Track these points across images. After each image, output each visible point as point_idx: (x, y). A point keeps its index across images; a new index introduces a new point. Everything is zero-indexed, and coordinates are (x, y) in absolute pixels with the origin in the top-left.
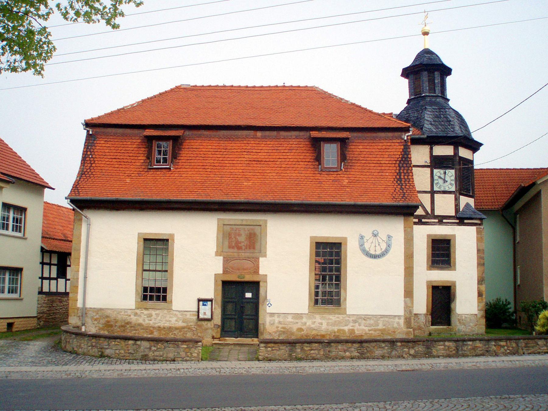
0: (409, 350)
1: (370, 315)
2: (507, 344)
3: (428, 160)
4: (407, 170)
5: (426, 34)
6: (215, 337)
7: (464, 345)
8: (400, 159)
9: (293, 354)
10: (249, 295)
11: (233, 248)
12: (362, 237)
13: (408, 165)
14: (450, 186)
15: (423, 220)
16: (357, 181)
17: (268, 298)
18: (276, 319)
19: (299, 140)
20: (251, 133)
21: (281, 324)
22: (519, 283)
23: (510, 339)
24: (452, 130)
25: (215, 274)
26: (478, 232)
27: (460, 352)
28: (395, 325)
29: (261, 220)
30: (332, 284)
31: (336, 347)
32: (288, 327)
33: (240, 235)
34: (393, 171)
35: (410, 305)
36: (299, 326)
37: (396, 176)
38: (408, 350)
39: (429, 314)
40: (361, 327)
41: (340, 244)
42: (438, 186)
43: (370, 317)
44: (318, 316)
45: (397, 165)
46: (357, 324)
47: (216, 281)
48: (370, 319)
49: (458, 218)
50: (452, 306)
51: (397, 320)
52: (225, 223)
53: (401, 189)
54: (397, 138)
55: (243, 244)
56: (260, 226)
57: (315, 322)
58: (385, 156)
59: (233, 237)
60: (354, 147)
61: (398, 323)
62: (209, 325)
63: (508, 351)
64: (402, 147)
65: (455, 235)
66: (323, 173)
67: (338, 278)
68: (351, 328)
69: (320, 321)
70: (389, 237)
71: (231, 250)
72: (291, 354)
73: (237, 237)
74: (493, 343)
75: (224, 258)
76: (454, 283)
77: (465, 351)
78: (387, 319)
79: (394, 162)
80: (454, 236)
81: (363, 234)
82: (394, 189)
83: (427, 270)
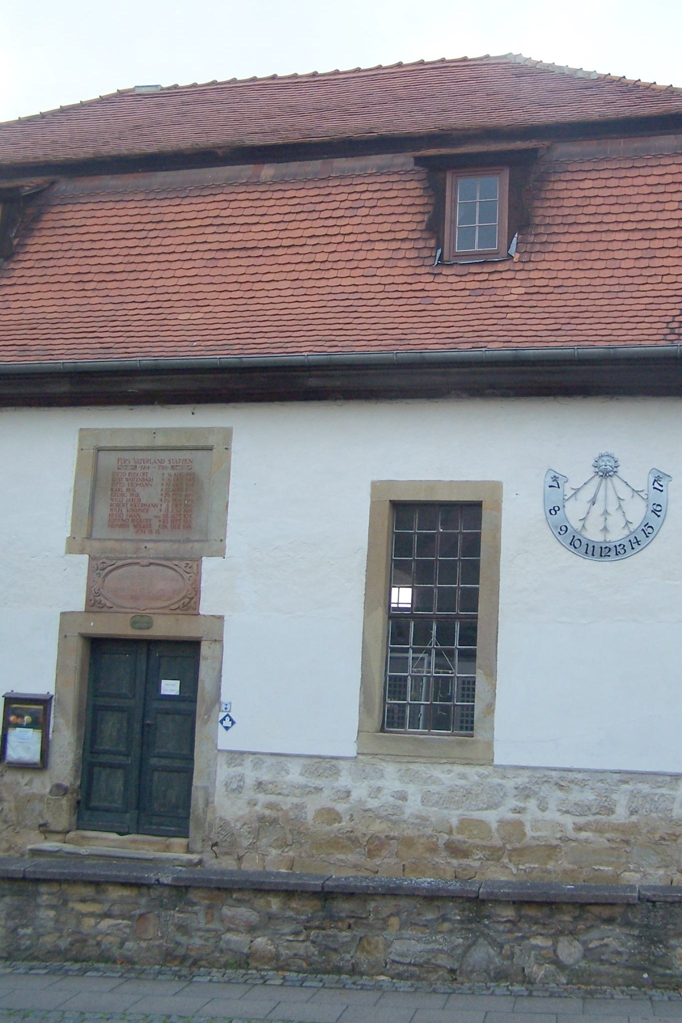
1: (579, 771)
6: (52, 827)
9: (22, 931)
10: (170, 687)
11: (121, 526)
12: (555, 479)
16: (557, 290)
17: (223, 699)
18: (250, 774)
19: (384, 179)
20: (246, 170)
21: (265, 792)
25: (63, 614)
29: (211, 430)
30: (450, 653)
31: (210, 907)
32: (287, 803)
33: (147, 482)
36: (323, 800)
41: (476, 507)
43: (580, 776)
44: (390, 769)
46: (532, 804)
47: (63, 636)
48: (582, 784)
52: (102, 444)
55: (154, 512)
56: (210, 449)
57: (379, 789)
58: (668, 206)
59: (124, 489)
60: (563, 185)
62: (41, 785)
66: (446, 271)
67: (470, 634)
68: (511, 816)
69: (398, 786)
70: (658, 481)
71: (118, 534)
72: (14, 930)
73: (138, 490)
75: (92, 559)
78: (645, 788)
81: (561, 470)
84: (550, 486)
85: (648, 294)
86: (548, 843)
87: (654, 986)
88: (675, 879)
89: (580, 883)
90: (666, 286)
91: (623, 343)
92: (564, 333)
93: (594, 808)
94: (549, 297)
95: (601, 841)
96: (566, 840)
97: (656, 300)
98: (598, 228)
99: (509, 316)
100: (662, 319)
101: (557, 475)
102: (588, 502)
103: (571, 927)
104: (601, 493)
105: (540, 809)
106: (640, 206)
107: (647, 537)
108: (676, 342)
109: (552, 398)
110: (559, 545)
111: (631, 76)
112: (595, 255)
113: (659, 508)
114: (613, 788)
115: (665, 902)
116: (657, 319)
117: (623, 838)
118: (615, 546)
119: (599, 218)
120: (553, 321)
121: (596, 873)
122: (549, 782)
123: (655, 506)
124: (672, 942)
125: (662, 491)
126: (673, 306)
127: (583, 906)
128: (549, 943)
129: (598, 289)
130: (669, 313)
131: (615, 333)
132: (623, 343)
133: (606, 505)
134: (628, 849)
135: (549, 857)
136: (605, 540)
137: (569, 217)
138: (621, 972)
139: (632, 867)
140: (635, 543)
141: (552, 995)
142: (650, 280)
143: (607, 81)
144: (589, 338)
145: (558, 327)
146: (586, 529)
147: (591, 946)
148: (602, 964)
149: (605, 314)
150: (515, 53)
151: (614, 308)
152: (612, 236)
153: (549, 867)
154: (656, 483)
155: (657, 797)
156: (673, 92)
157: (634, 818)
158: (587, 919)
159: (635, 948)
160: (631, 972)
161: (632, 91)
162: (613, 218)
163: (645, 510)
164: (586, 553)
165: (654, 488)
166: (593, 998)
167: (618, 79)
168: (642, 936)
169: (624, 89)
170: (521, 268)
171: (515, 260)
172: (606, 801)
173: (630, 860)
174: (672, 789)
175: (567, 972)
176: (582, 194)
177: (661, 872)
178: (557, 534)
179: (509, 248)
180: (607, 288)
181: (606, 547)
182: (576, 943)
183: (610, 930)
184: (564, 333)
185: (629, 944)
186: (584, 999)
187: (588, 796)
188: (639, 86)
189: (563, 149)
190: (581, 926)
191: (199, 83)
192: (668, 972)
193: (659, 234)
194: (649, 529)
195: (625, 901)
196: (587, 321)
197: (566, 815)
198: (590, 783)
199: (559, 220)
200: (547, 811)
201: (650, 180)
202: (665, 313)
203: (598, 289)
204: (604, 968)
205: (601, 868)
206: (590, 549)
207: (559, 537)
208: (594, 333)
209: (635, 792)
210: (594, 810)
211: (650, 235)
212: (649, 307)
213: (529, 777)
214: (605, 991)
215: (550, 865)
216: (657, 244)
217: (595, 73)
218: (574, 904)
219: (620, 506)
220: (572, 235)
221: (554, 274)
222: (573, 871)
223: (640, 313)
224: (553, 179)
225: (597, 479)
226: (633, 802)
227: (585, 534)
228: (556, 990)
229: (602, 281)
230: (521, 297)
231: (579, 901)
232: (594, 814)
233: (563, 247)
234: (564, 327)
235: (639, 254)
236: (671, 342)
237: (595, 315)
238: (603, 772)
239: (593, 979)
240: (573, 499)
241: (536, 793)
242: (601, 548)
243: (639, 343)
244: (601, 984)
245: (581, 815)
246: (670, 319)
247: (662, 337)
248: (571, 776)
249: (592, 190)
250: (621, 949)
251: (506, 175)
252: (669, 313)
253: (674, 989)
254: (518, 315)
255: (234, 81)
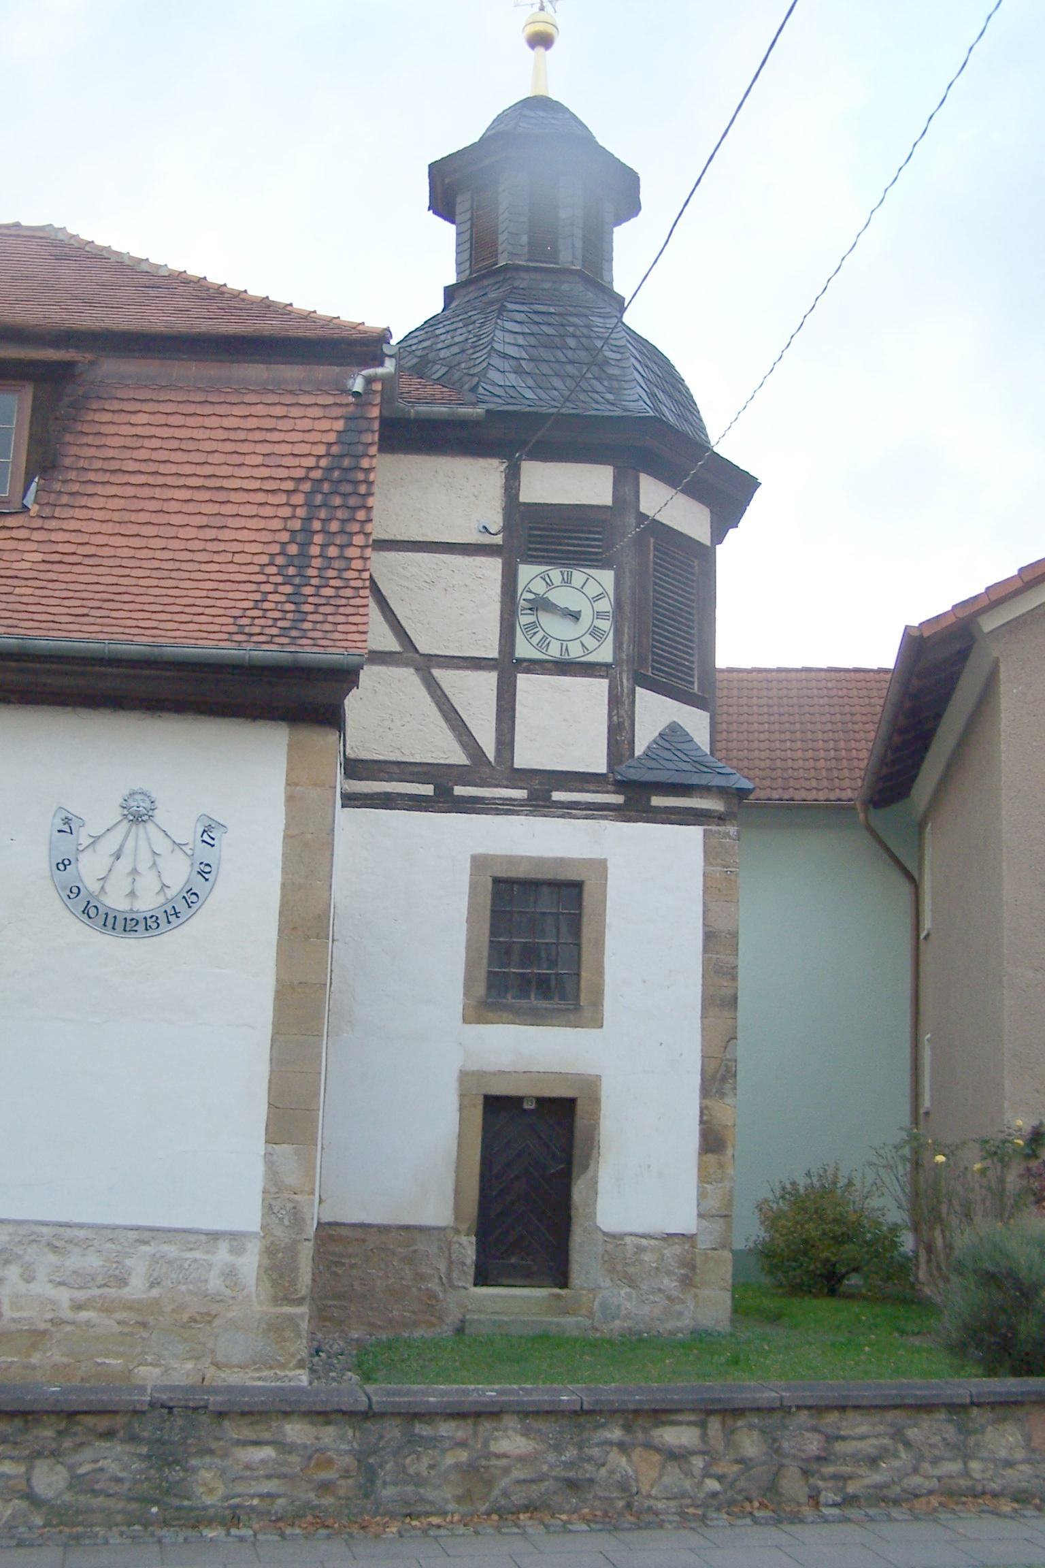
0: (30, 1468)
1: (81, 1226)
2: (704, 1437)
3: (495, 520)
4: (344, 521)
5: (541, 41)
7: (412, 1441)
8: (317, 474)
12: (67, 821)
13: (352, 501)
14: (590, 642)
15: (459, 790)
22: (927, 1102)
23: (732, 1412)
24: (609, 396)
26: (711, 853)
27: (388, 1492)
28: (215, 1283)
34: (277, 524)
35: (292, 1178)
37: (284, 544)
38: (20, 1469)
39: (464, 1227)
40: (37, 1288)
42: (535, 640)
43: (82, 1234)
45: (298, 499)
48: (85, 1245)
49: (622, 786)
50: (578, 1192)
51: (223, 1254)
53: (296, 598)
54: (321, 389)
58: (249, 460)
61: (230, 1274)
63: (712, 1485)
64: (339, 425)
65: (605, 861)
70: (209, 832)
74: (616, 1434)
76: (592, 1085)
77: (419, 1481)
78: (171, 1250)
79: (289, 485)
80: (601, 866)
81: (76, 809)
82: (258, 596)
83: (466, 1020)
84: (59, 831)
85: (213, 576)
86: (34, 1328)
87: (166, 1523)
88: (208, 1376)
89: (76, 1382)
90: (237, 568)
91: (173, 641)
92: (91, 620)
93: (100, 1277)
94: (75, 569)
95: (108, 1324)
96: (57, 1322)
97: (222, 586)
98: (151, 480)
99: (17, 591)
100: (228, 612)
101: (70, 816)
102: (111, 855)
103: (54, 1445)
104: (130, 844)
105: (24, 1280)
106: (210, 456)
107: (190, 907)
108: (244, 644)
109: (69, 709)
110: (67, 913)
111: (215, 278)
112: (144, 517)
113: (207, 869)
114: (128, 1250)
115: (187, 1407)
116: (221, 612)
117: (140, 1319)
118: (145, 918)
119: (153, 467)
120: (78, 603)
121: (99, 1368)
122: (39, 1241)
123: (202, 866)
124: (194, 1462)
125: (213, 846)
126: (244, 596)
127: (71, 1415)
128: (22, 1469)
129: (145, 564)
130: (239, 604)
131: (162, 625)
132: (173, 641)
133: (135, 860)
134: (145, 1335)
135: (34, 1347)
136: (131, 910)
137: (112, 462)
138: (121, 1505)
139: (149, 1358)
140: (173, 914)
141: (21, 1544)
142: (216, 558)
143: (180, 281)
144: (127, 631)
145: (85, 611)
146: (106, 893)
147: (81, 1471)
148: (97, 1497)
149: (152, 599)
150: (57, 225)
151: (164, 592)
152: (169, 493)
153: (33, 1360)
154: (205, 834)
155: (188, 1262)
156: (269, 307)
157: (155, 1292)
158: (75, 1434)
159: (141, 1472)
160: (134, 1506)
161: (213, 298)
162: (173, 469)
163: (189, 869)
164: (105, 925)
165: (203, 841)
166: (79, 1544)
167: (196, 280)
168: (152, 1456)
169: (203, 295)
170: (39, 526)
171: (32, 513)
172: (116, 1268)
173: (147, 1350)
174: (208, 1252)
175: (44, 1509)
176: (134, 431)
177: (190, 1365)
178: (65, 898)
179: (24, 496)
180: (157, 564)
181: (132, 919)
182: (59, 1468)
183: (107, 1448)
184: (91, 620)
185: (134, 1466)
186: (66, 1546)
187: (93, 1262)
188: (223, 293)
189: (111, 367)
190: (67, 1443)
191: (24, 223)
192: (186, 1503)
193: (234, 497)
194: (194, 896)
195: (131, 1408)
196: (126, 607)
197: (62, 1288)
198: (96, 1243)
199: (98, 464)
200: (35, 1282)
201: (227, 422)
202: (232, 604)
203: (145, 564)
204: (96, 1502)
205: (107, 1361)
206: (110, 921)
207: (68, 902)
208: (134, 623)
209: (158, 1255)
210: (100, 1281)
211: (222, 496)
212: (211, 594)
213: (10, 1235)
214: (96, 1535)
215: (35, 1359)
216: (229, 509)
217: (165, 269)
218: (57, 1413)
219: (155, 863)
220: (115, 487)
221: (85, 538)
222: (67, 1366)
223: (198, 602)
224: (94, 406)
225: (125, 825)
226: (154, 1270)
227: (102, 898)
228: (26, 1536)
229: (150, 554)
230: (36, 566)
231: (66, 1408)
232: (99, 1287)
233: (100, 502)
234: (93, 612)
235: (203, 521)
236: (237, 644)
237: (138, 599)
238: (115, 1228)
239: (81, 1518)
240: (90, 849)
241: (19, 1257)
242: (126, 919)
243: (193, 641)
244: (92, 1525)
245: (81, 1288)
246: (239, 613)
247: (225, 636)
248: (69, 1233)
249: (148, 427)
250: (123, 1475)
251: (28, 392)
252: (239, 604)
253: (194, 1527)
254: (29, 591)
255: (17, 225)
